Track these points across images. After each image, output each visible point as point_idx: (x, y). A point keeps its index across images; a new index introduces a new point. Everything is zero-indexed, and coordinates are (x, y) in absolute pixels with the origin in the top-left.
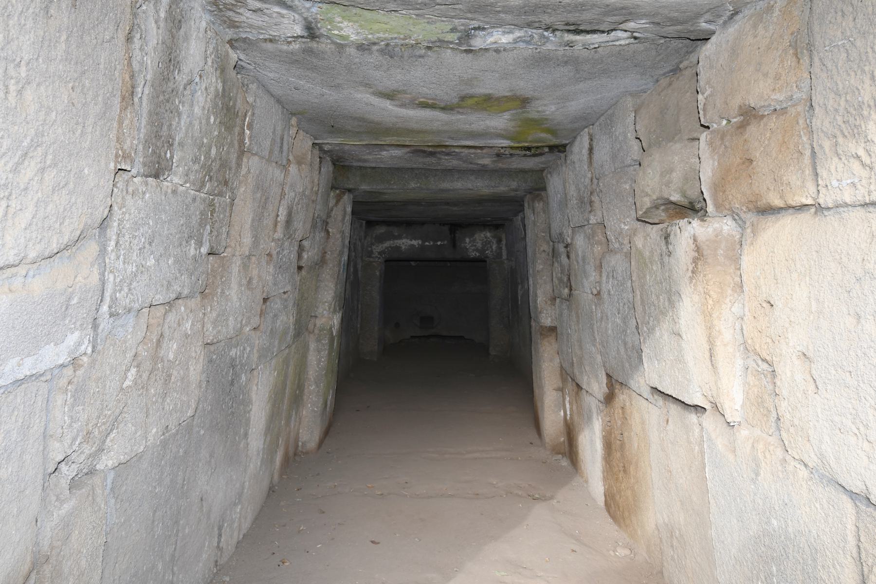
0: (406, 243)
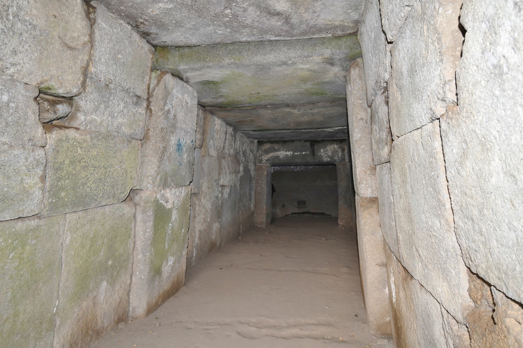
0: (283, 154)
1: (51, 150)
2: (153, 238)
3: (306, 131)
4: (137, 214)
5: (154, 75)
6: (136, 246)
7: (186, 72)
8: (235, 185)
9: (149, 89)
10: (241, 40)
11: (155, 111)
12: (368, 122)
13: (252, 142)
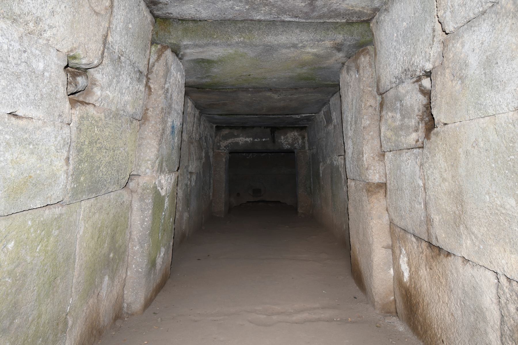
0: (243, 140)
1: (75, 129)
2: (152, 227)
3: (274, 116)
4: (133, 202)
5: (153, 49)
6: (132, 236)
7: (186, 48)
9: (148, 64)
10: (255, 18)
11: (155, 89)
12: (377, 109)
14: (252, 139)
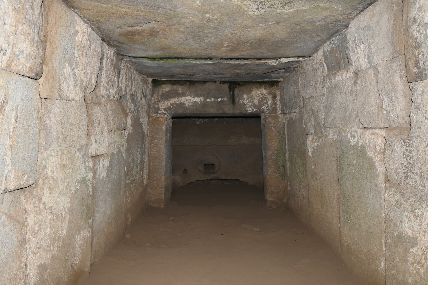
0: (190, 100)
8: (119, 151)
13: (145, 81)
14: (202, 99)
